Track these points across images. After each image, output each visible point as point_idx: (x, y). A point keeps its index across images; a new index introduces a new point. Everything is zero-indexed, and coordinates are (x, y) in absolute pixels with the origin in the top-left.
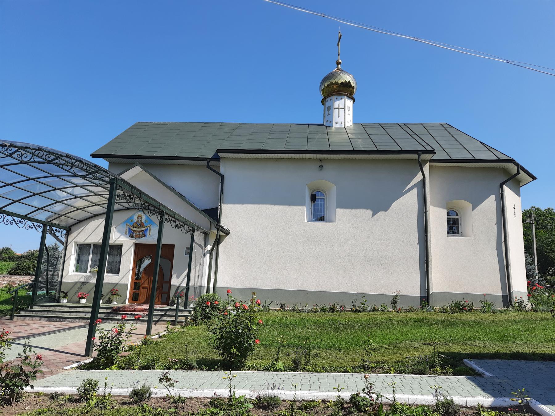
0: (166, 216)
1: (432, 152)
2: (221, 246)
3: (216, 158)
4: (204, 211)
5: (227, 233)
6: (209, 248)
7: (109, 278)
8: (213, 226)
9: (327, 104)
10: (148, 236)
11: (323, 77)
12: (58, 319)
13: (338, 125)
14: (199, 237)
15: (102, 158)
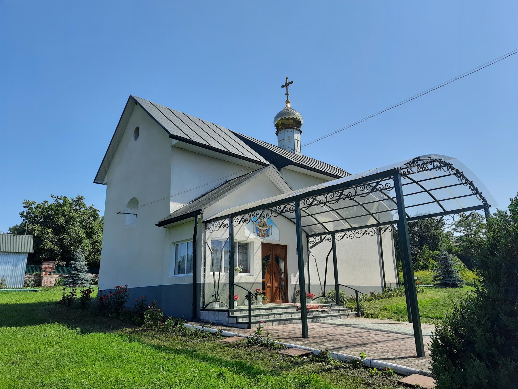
7: (240, 278)
10: (270, 236)
12: (286, 322)
15: (247, 157)
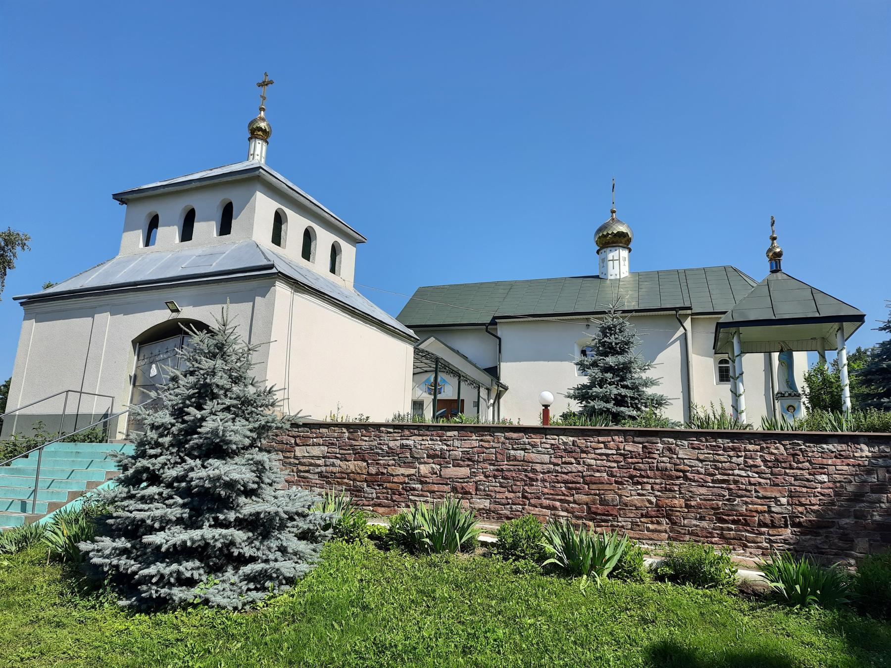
0: (462, 378)
1: (690, 308)
2: (501, 400)
3: (493, 322)
5: (506, 389)
6: (492, 401)
8: (494, 383)
9: (602, 255)
10: (443, 393)
11: (598, 227)
13: (612, 278)
14: (483, 393)
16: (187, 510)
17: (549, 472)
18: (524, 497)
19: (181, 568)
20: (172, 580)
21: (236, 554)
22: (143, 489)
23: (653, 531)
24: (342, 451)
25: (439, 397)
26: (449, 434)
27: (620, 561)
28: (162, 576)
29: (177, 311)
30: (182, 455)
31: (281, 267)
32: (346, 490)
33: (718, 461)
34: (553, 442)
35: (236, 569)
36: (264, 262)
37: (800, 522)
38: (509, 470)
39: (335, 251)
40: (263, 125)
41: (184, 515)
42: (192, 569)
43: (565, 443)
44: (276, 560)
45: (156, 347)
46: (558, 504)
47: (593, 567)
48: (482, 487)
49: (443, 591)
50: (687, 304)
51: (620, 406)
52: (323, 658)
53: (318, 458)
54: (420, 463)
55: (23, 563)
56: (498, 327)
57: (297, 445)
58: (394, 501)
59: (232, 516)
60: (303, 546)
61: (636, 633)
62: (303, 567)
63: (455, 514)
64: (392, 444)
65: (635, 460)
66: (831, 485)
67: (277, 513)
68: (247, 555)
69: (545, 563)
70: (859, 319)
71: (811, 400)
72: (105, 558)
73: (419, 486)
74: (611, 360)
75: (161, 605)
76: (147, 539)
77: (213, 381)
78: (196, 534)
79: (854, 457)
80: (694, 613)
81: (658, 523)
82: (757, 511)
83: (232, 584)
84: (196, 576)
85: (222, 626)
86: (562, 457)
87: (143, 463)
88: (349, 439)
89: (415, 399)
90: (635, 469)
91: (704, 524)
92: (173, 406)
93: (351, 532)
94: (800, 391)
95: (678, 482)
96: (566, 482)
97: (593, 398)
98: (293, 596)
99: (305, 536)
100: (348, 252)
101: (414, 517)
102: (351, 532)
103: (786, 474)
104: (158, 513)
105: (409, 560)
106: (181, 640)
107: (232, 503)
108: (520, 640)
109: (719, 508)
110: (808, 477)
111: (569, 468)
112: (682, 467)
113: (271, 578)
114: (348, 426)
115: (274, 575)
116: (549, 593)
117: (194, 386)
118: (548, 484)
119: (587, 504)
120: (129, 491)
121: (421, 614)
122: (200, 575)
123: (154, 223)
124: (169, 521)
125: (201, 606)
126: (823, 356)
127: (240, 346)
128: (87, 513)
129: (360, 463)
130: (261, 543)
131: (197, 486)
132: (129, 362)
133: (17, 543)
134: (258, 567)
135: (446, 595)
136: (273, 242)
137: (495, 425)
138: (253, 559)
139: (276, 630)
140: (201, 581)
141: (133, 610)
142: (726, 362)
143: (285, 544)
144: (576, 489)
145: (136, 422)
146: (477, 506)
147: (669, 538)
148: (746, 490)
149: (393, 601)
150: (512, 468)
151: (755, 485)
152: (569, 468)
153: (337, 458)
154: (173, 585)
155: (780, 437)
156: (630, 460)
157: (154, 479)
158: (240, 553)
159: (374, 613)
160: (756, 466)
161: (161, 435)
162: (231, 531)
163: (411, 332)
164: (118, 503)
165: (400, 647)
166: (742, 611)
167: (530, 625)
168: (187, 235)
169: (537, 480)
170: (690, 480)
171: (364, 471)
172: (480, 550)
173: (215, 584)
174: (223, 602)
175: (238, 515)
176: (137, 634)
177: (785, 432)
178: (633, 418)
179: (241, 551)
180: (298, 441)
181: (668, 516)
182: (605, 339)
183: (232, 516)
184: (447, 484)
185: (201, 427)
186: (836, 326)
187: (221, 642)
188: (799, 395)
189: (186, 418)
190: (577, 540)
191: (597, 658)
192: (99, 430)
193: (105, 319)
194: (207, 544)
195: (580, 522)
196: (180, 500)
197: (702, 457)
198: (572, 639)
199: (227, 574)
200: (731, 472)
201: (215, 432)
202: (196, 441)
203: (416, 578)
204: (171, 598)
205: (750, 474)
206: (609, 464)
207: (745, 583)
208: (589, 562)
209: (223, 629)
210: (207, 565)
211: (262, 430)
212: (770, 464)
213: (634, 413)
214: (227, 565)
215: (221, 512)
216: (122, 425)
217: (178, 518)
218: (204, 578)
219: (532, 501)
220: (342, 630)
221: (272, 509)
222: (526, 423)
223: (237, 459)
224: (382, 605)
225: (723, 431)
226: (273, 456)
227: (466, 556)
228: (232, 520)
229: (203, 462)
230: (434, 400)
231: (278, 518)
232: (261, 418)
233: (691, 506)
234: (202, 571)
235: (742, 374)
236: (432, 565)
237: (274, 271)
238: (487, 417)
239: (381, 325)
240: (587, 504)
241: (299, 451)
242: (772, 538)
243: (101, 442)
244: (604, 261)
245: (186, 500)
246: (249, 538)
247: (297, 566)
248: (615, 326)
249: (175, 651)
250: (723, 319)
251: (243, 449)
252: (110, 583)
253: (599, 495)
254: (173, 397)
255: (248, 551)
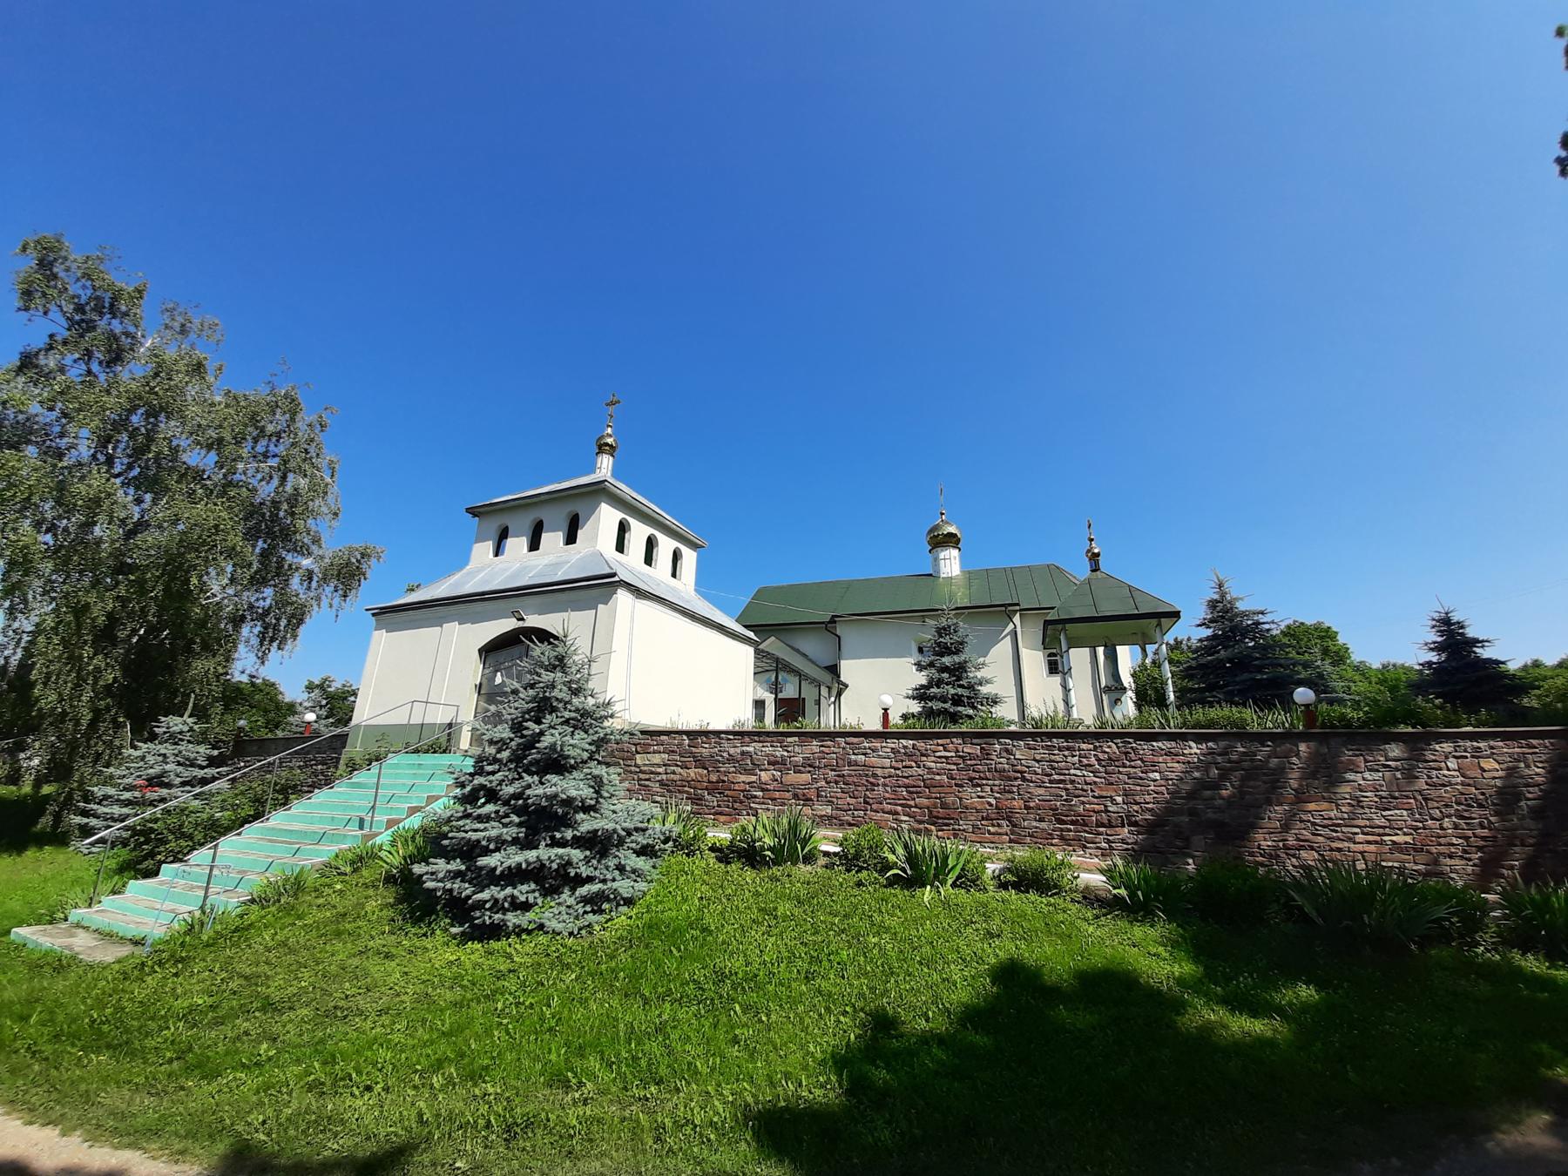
1: (1018, 605)
2: (842, 698)
3: (833, 620)
4: (825, 667)
6: (833, 699)
14: (824, 691)
16: (523, 830)
17: (890, 776)
18: (866, 802)
19: (516, 892)
20: (506, 905)
21: (572, 874)
22: (480, 807)
23: (993, 834)
24: (683, 759)
25: (780, 696)
26: (789, 739)
27: (963, 869)
28: (496, 901)
29: (522, 619)
30: (520, 770)
31: (623, 575)
32: (687, 798)
33: (1054, 761)
34: (893, 746)
35: (573, 890)
36: (607, 571)
37: (1136, 821)
38: (850, 776)
39: (676, 556)
40: (610, 441)
41: (520, 835)
42: (527, 892)
43: (905, 747)
44: (614, 880)
45: (502, 655)
46: (899, 808)
47: (936, 877)
48: (823, 793)
49: (784, 908)
50: (1015, 601)
51: (958, 706)
52: (660, 990)
53: (659, 765)
54: (761, 770)
55: (356, 885)
56: (837, 625)
57: (638, 753)
58: (735, 809)
59: (569, 834)
60: (641, 863)
61: (983, 950)
62: (642, 886)
63: (796, 824)
64: (732, 751)
65: (973, 762)
66: (1163, 782)
67: (615, 831)
68: (584, 875)
69: (888, 874)
70: (1176, 615)
71: (1137, 693)
72: (439, 881)
73: (760, 794)
74: (947, 660)
75: (495, 932)
76: (483, 861)
77: (553, 694)
78: (532, 855)
79: (1184, 755)
80: (1040, 925)
81: (999, 825)
82: (1094, 811)
83: (568, 907)
84: (531, 900)
85: (557, 954)
86: (902, 761)
87: (479, 780)
88: (689, 746)
89: (757, 698)
90: (974, 771)
91: (1043, 825)
92: (513, 720)
93: (691, 845)
94: (1126, 684)
95: (1016, 783)
96: (906, 786)
97: (931, 699)
98: (631, 918)
99: (645, 851)
100: (689, 557)
101: (755, 828)
102: (691, 845)
103: (1120, 772)
104: (494, 833)
105: (749, 874)
106: (514, 971)
107: (569, 819)
108: (865, 961)
109: (1057, 809)
110: (1141, 775)
111: (909, 772)
112: (1019, 767)
113: (608, 900)
114: (688, 733)
115: (612, 896)
116: (893, 906)
117: (534, 699)
118: (889, 789)
119: (928, 808)
120: (465, 810)
121: (763, 934)
122: (535, 898)
123: (504, 535)
124: (504, 842)
125: (536, 932)
126: (1144, 650)
127: (581, 657)
128: (424, 830)
129: (700, 770)
130: (599, 862)
131: (533, 804)
132: (474, 670)
133: (352, 863)
134: (595, 887)
135: (788, 913)
136: (617, 550)
137: (838, 730)
138: (590, 880)
139: (612, 957)
140: (537, 904)
141: (465, 938)
142: (1055, 655)
143: (623, 862)
144: (917, 793)
145: (477, 738)
146: (819, 813)
147: (1011, 841)
148: (1083, 790)
149: (733, 921)
150: (853, 773)
151: (1090, 784)
152: (909, 772)
153: (677, 766)
154: (508, 910)
155: (1112, 736)
156: (969, 762)
157: (492, 796)
158: (576, 873)
159: (714, 935)
160: (1091, 766)
161: (499, 751)
162: (568, 850)
163: (751, 635)
164: (454, 823)
165: (740, 976)
166: (1085, 920)
167: (875, 944)
168: (534, 545)
169: (878, 785)
170: (1028, 780)
171: (705, 779)
172: (822, 861)
173: (551, 907)
174: (559, 927)
175: (575, 832)
176: (468, 965)
177: (1116, 730)
178: (970, 717)
179: (578, 870)
180: (639, 749)
181: (1009, 819)
182: (941, 640)
183: (569, 834)
184: (788, 791)
185: (539, 742)
186: (1154, 622)
187: (555, 972)
188: (1125, 688)
189: (525, 732)
190: (920, 849)
191: (944, 980)
192: (443, 740)
193: (453, 628)
194: (543, 865)
195: (921, 826)
196: (516, 819)
197: (1038, 757)
198: (918, 958)
199: (564, 896)
200: (1067, 772)
201: (553, 747)
202: (534, 756)
203: (757, 894)
204: (505, 925)
205: (1086, 773)
206: (948, 766)
207: (1087, 887)
208: (933, 872)
209: (557, 957)
210: (543, 887)
211: (600, 743)
212: (1103, 763)
213: (971, 712)
214: (563, 886)
215: (558, 831)
216: (465, 742)
217: (514, 838)
218: (540, 901)
219: (874, 806)
220: (681, 957)
221: (610, 826)
222: (867, 728)
223: (575, 774)
224: (723, 926)
225: (1057, 730)
226: (612, 770)
227: (809, 868)
228: (569, 838)
229: (541, 778)
230: (775, 699)
231: (615, 836)
232: (600, 730)
233: (1030, 808)
234: (537, 894)
235: (1070, 669)
236: (776, 879)
237: (616, 579)
238: (828, 721)
239: (721, 628)
240: (928, 808)
241: (639, 759)
242: (1110, 838)
243: (444, 752)
244: (936, 560)
245: (522, 819)
246: (586, 857)
247: (636, 884)
248: (949, 627)
249: (506, 984)
250: (1052, 616)
251: (581, 763)
252: (442, 908)
253: (939, 798)
254: (513, 711)
255: (585, 871)
